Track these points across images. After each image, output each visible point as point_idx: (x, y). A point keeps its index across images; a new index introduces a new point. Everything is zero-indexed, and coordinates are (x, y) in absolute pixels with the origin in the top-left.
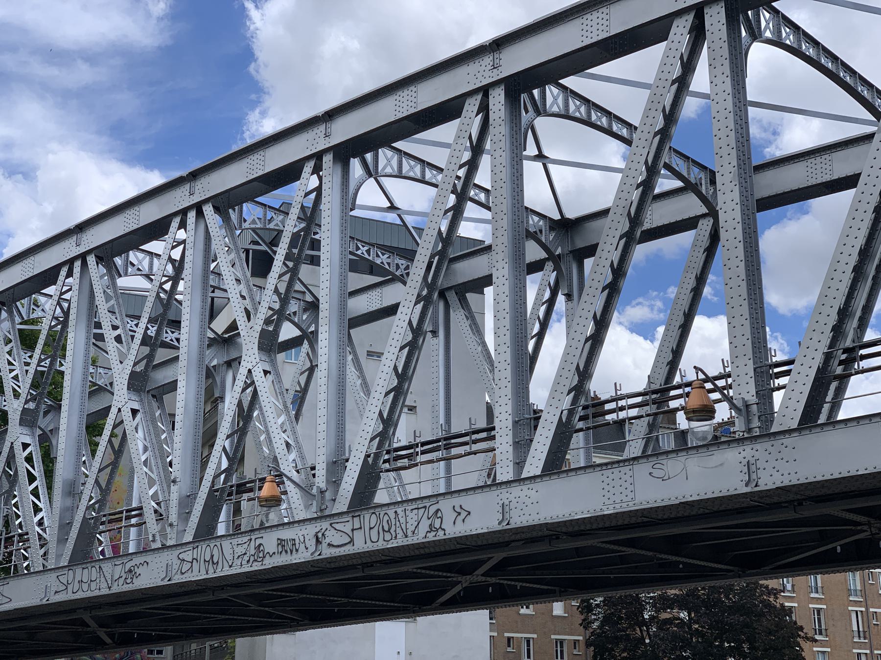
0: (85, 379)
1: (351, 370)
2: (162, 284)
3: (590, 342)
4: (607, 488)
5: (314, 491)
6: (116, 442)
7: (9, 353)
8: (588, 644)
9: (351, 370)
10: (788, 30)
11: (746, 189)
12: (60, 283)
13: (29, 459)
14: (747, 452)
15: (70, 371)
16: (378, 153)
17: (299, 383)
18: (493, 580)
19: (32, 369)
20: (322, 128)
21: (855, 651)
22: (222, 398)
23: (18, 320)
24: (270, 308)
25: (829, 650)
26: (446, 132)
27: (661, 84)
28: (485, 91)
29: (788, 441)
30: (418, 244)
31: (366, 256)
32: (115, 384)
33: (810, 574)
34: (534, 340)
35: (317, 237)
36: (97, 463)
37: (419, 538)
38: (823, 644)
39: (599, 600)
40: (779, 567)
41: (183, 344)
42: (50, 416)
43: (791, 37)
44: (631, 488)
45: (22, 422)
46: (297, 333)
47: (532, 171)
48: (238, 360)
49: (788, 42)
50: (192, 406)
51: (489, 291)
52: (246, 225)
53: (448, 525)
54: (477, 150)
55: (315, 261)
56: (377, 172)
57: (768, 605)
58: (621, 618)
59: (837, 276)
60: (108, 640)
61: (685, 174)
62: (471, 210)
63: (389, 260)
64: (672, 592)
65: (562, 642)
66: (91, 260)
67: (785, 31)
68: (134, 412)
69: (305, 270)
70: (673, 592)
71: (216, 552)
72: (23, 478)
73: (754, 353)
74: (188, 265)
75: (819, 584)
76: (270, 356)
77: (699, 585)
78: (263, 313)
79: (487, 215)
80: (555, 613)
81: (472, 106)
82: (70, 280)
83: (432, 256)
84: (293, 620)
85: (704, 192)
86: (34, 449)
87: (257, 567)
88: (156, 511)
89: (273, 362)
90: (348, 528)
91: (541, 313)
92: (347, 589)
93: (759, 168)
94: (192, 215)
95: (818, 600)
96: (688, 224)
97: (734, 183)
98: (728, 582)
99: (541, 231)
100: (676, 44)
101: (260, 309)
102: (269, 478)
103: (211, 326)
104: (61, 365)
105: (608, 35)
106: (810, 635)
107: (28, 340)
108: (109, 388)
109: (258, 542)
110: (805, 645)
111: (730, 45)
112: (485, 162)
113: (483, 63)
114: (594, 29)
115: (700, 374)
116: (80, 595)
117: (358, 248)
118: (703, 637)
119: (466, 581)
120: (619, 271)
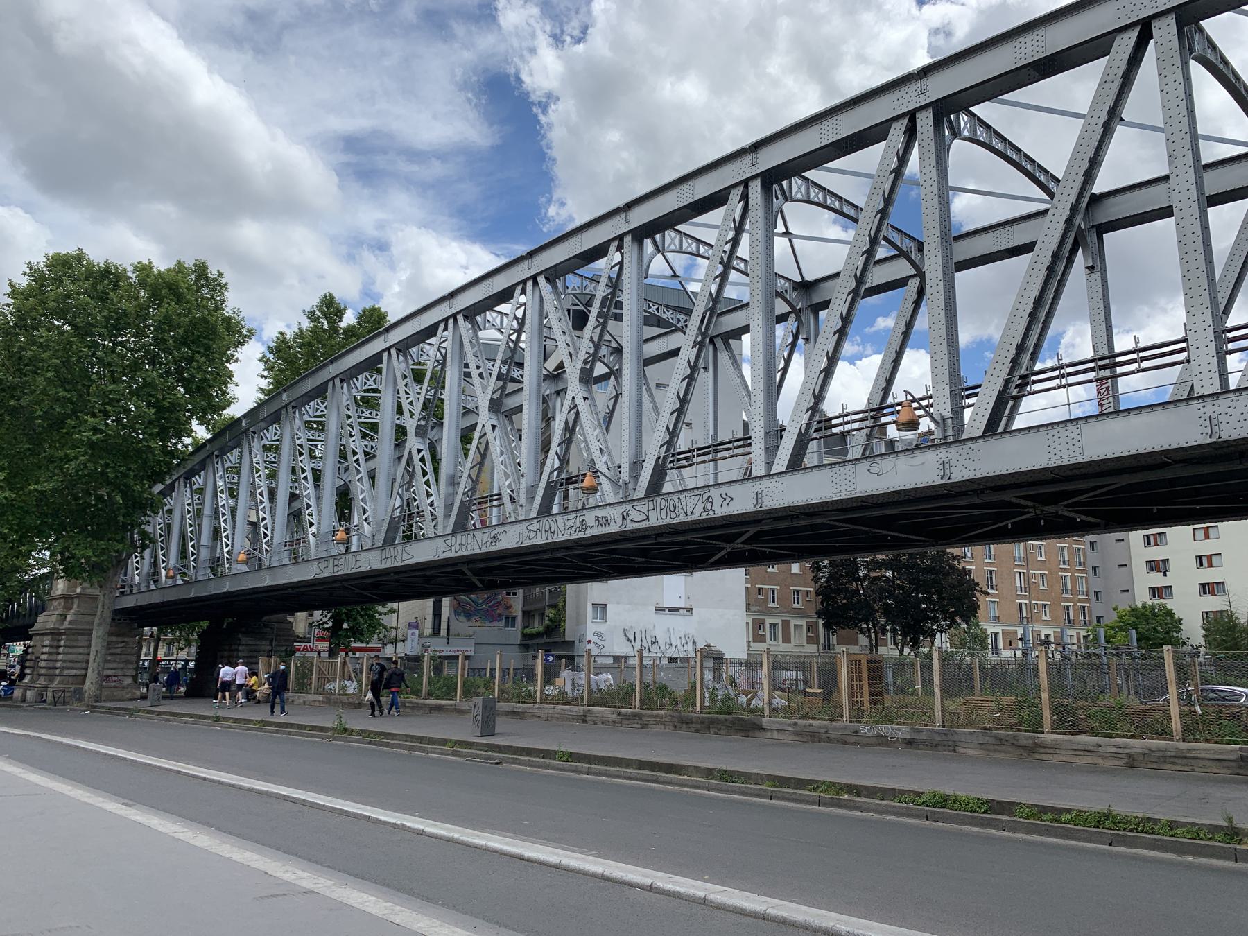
29: (974, 445)
38: (993, 596)
57: (952, 567)
67: (979, 130)
85: (913, 258)
93: (956, 239)
96: (900, 283)
98: (924, 549)
105: (841, 137)
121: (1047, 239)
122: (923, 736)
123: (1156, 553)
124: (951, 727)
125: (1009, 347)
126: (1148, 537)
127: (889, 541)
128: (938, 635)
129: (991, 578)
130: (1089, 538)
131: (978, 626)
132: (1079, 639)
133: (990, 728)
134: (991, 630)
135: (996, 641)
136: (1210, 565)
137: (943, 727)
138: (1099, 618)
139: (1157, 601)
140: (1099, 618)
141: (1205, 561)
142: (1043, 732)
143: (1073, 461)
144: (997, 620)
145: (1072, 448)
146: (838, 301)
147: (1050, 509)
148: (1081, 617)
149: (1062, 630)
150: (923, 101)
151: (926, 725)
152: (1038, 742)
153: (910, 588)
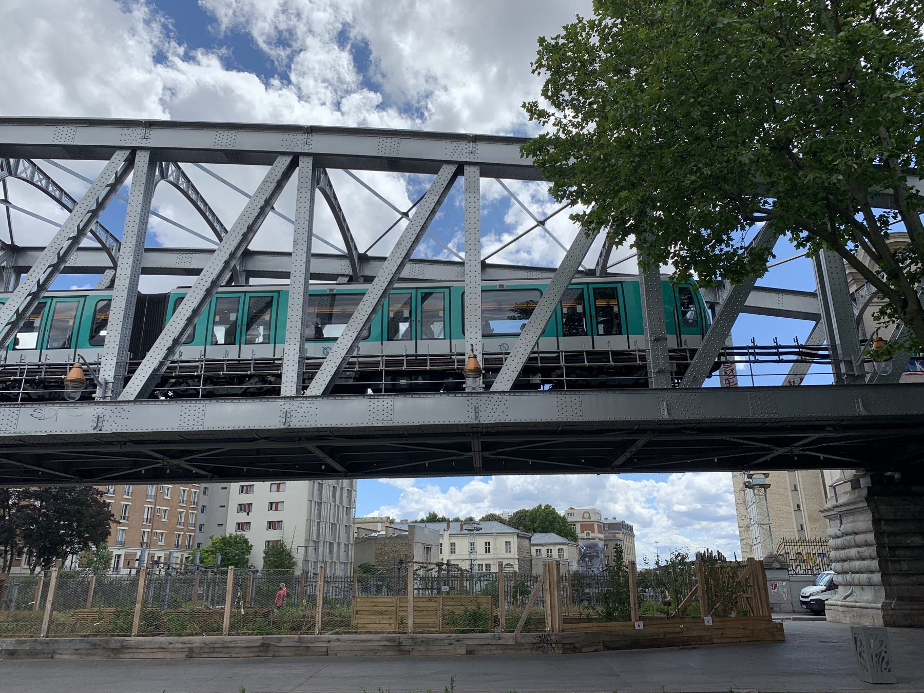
29: (126, 407)
38: (124, 525)
40: (104, 479)
57: (96, 501)
64: (32, 489)
67: (181, 180)
70: (34, 488)
75: (131, 491)
77: (52, 486)
85: (113, 254)
93: (147, 250)
96: (100, 270)
98: (73, 485)
105: (72, 143)
106: (117, 519)
110: (113, 525)
111: (147, 177)
115: (81, 359)
121: (211, 270)
122: (27, 647)
123: (245, 499)
124: (55, 637)
125: (168, 338)
126: (242, 487)
127: (39, 476)
128: (70, 557)
129: (125, 511)
130: (203, 485)
131: (105, 549)
132: (182, 560)
133: (88, 636)
134: (116, 552)
135: (118, 561)
136: (276, 509)
137: (47, 637)
138: (199, 544)
139: (239, 533)
140: (199, 544)
141: (274, 505)
142: (130, 636)
143: (195, 429)
144: (123, 544)
145: (197, 420)
146: (38, 270)
147: (175, 462)
148: (187, 544)
149: (170, 553)
150: (144, 144)
151: (31, 637)
152: (125, 644)
153: (54, 516)
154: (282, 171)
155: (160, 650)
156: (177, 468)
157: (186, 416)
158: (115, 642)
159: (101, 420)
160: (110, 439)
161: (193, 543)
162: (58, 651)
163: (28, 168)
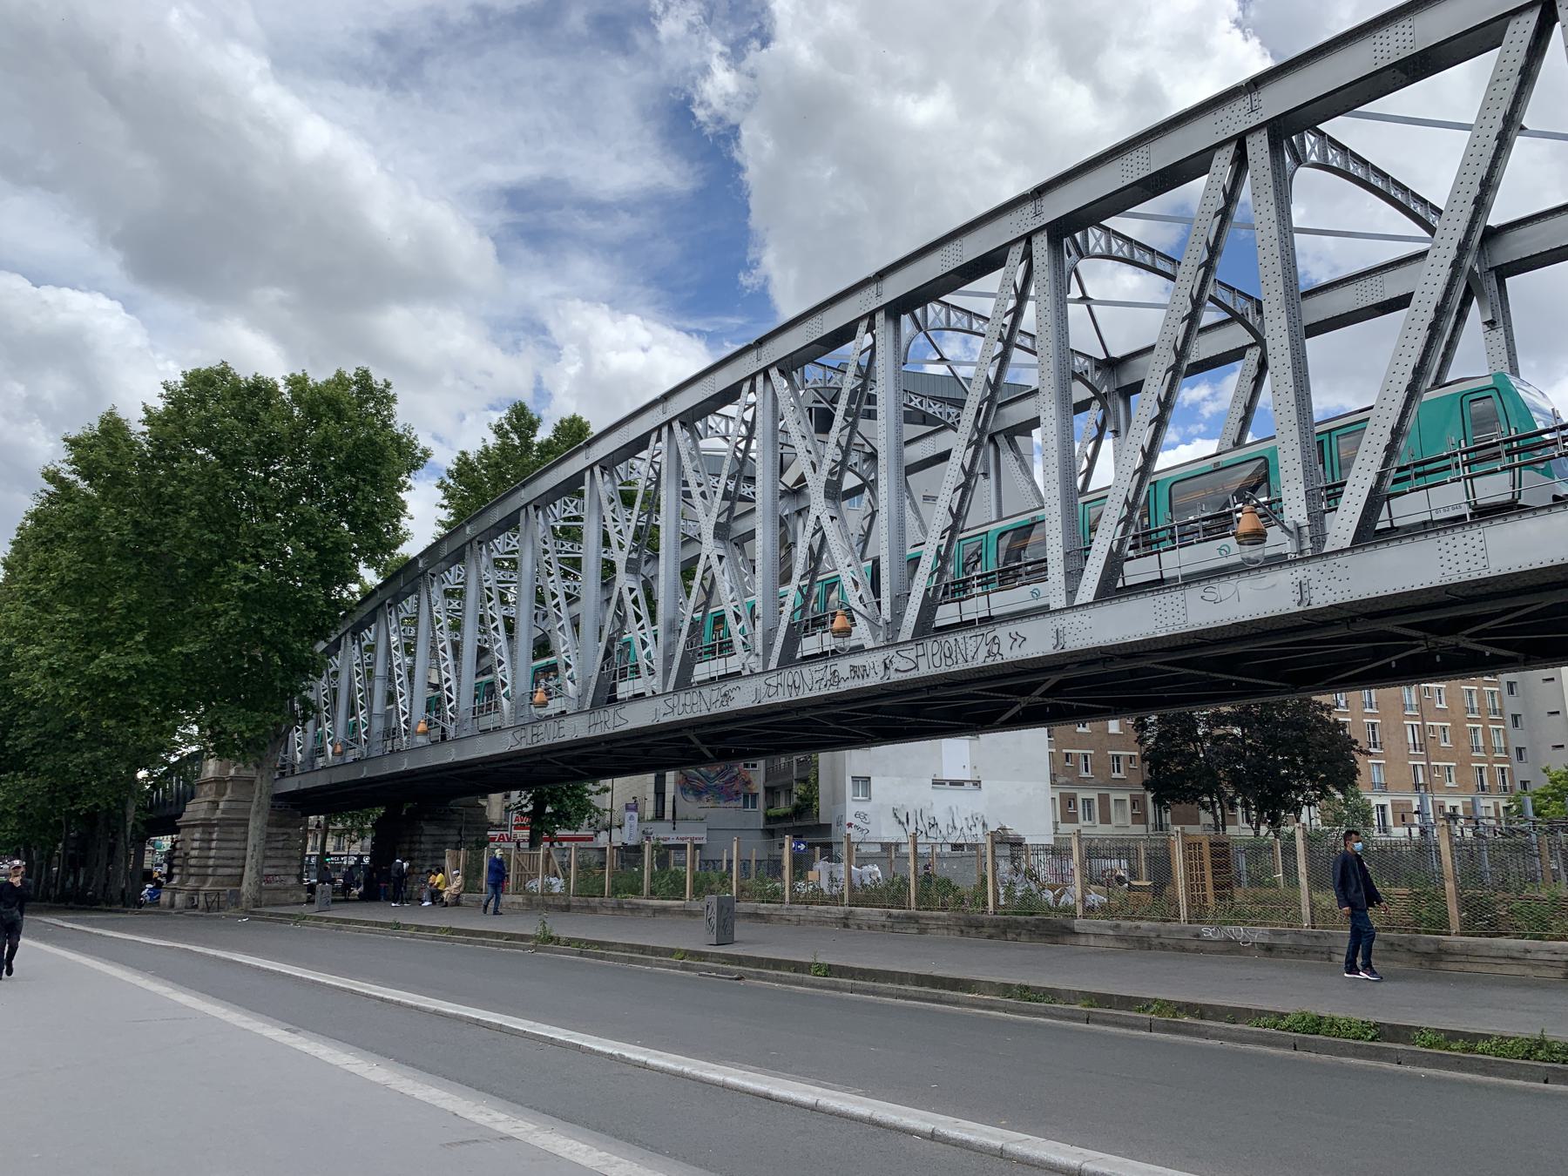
0: (677, 531)
1: (909, 512)
2: (737, 444)
3: (1138, 474)
4: (1159, 612)
5: (881, 623)
6: (707, 584)
7: (613, 511)
8: (1144, 759)
9: (909, 512)
10: (1334, 152)
11: (1293, 314)
12: (651, 447)
13: (635, 601)
14: (1299, 572)
15: (664, 524)
16: (926, 311)
17: (862, 527)
18: (1050, 701)
19: (633, 524)
20: (874, 288)
21: (1410, 763)
22: (794, 544)
23: (618, 482)
24: (833, 460)
25: (1384, 762)
26: (991, 282)
27: (1204, 217)
28: (1028, 238)
29: (1340, 560)
30: (967, 393)
31: (919, 407)
32: (703, 534)
33: (1364, 689)
34: (1083, 475)
35: (872, 392)
36: (691, 603)
37: (979, 662)
39: (1154, 718)
41: (758, 497)
42: (650, 565)
43: (1338, 159)
44: (1183, 611)
45: (628, 570)
46: (859, 482)
47: (1076, 311)
48: (807, 509)
49: (1335, 164)
50: (769, 550)
51: (1036, 433)
52: (808, 385)
53: (1005, 650)
54: (1022, 297)
55: (871, 415)
56: (926, 327)
57: (1321, 720)
58: (1174, 735)
59: (1390, 396)
60: (710, 755)
61: (1231, 306)
62: (1017, 355)
63: (941, 410)
64: (1225, 709)
65: (1118, 758)
66: (676, 425)
68: (721, 558)
69: (863, 424)
71: (797, 678)
72: (631, 618)
73: (1303, 457)
74: (758, 425)
75: (1374, 700)
76: (835, 503)
78: (827, 465)
79: (1032, 359)
80: (1110, 731)
81: (1016, 253)
82: (659, 444)
83: (982, 403)
84: (868, 737)
85: (1251, 322)
86: (640, 593)
87: (833, 690)
88: (744, 643)
89: (838, 509)
90: (912, 655)
91: (1089, 451)
92: (914, 710)
94: (760, 379)
95: (1371, 715)
96: (1238, 354)
97: (1280, 310)
98: (1281, 698)
99: (1087, 372)
100: (1217, 177)
101: (824, 461)
102: (839, 612)
103: (783, 479)
104: (657, 520)
107: (628, 500)
108: (698, 538)
109: (833, 668)
110: (1360, 758)
111: (1274, 173)
112: (1030, 309)
113: (1025, 212)
114: (1134, 168)
116: (684, 716)
117: (911, 400)
118: (1256, 752)
119: (1024, 702)
120: (1166, 404)
122: (1287, 941)
124: (1324, 928)
127: (1234, 688)
128: (1305, 809)
129: (1374, 733)
130: (1505, 677)
131: (1358, 797)
132: (1497, 811)
134: (1376, 801)
135: (1383, 816)
140: (1524, 784)
143: (1475, 576)
144: (1384, 788)
150: (1255, 120)
154: (1524, 47)
155: (1510, 961)
156: (1455, 651)
157: (1450, 556)
158: (1426, 940)
159: (1305, 588)
160: (1329, 617)
161: (1512, 781)
162: (1334, 950)
163: (1101, 236)
